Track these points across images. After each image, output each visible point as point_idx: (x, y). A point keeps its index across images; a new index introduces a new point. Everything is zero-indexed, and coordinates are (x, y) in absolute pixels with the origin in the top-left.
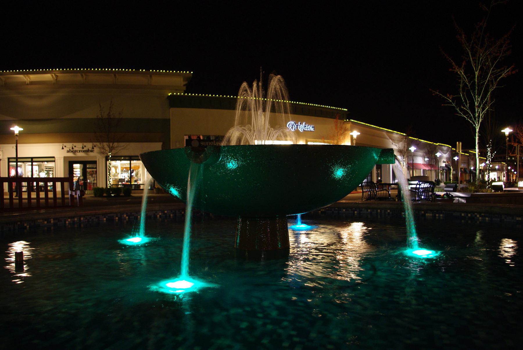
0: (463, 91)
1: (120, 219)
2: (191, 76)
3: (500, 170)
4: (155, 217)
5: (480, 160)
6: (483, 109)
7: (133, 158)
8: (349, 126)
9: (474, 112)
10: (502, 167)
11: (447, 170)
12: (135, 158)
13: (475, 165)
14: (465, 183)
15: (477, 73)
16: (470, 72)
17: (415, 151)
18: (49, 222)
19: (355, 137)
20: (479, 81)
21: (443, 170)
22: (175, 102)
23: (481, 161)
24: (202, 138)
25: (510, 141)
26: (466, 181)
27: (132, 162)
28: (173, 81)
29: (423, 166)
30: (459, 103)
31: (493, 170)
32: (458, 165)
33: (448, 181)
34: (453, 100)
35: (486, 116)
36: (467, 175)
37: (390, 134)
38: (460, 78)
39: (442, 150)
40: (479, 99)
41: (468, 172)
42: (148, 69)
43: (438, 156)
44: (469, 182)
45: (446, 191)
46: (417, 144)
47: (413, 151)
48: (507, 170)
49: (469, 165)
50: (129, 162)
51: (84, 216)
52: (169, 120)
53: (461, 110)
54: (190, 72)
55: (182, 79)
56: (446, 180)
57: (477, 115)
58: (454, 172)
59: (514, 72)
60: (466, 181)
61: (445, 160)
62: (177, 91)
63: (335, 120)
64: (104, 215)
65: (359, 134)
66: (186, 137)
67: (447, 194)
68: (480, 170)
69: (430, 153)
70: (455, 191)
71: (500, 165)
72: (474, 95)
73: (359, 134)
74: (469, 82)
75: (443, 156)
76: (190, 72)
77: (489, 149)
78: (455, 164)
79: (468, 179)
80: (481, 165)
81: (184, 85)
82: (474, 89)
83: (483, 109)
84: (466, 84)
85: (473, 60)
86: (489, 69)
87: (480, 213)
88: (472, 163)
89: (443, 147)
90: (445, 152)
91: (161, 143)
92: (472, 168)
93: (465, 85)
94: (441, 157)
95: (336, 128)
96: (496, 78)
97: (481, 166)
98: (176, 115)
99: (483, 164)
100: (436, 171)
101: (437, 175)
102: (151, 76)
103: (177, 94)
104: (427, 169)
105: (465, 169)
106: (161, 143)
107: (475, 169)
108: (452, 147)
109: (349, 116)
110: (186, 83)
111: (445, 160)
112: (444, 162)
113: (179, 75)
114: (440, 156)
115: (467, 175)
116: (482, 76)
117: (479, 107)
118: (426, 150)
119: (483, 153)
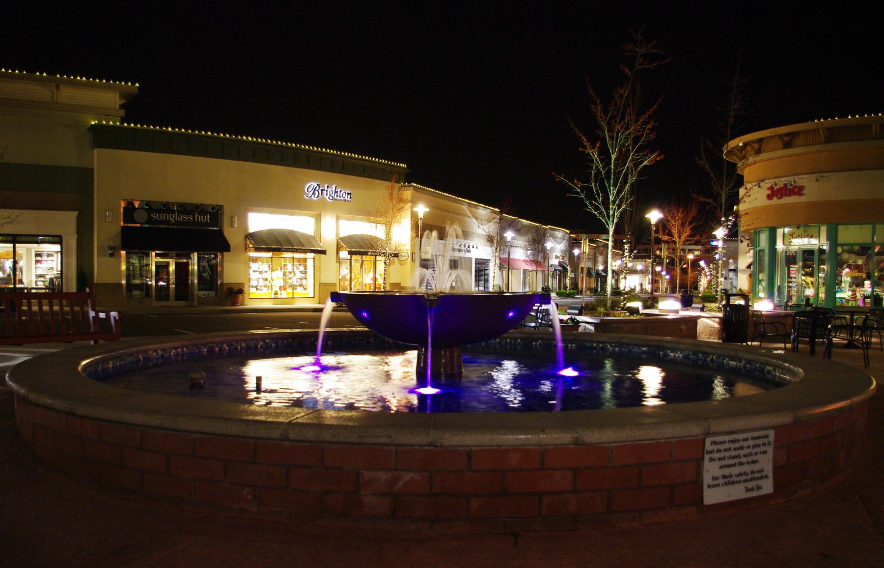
0: (595, 182)
1: (221, 350)
2: (136, 91)
3: (643, 272)
4: (256, 347)
5: (613, 253)
6: (619, 207)
7: (19, 239)
8: (408, 193)
9: (607, 209)
10: (646, 267)
11: (562, 271)
12: (24, 239)
13: (606, 263)
14: (588, 292)
15: (613, 157)
16: (606, 160)
17: (513, 238)
18: (157, 354)
19: (421, 215)
20: (616, 167)
21: (555, 270)
22: (103, 137)
23: (615, 255)
24: (137, 205)
25: (657, 232)
26: (590, 289)
27: (17, 245)
28: (101, 100)
29: (524, 264)
30: (591, 196)
31: (633, 271)
32: (578, 264)
33: (562, 291)
34: (582, 189)
35: (621, 218)
36: (593, 280)
37: (473, 209)
38: (592, 161)
39: (554, 237)
40: (615, 192)
41: (594, 274)
42: (51, 73)
43: (548, 248)
44: (594, 291)
45: (569, 314)
46: (519, 231)
47: (509, 239)
48: (654, 273)
49: (595, 262)
50: (10, 246)
51: (186, 347)
52: (91, 171)
53: (591, 204)
54: (133, 84)
55: (117, 96)
56: (559, 289)
57: (611, 213)
58: (573, 275)
59: (658, 159)
60: (590, 289)
61: (559, 254)
62: (107, 116)
63: (389, 184)
64: (205, 345)
65: (428, 210)
66: (123, 204)
67: (571, 319)
68: (613, 271)
69: (537, 243)
70: (580, 314)
71: (643, 263)
72: (609, 185)
73: (428, 210)
74: (604, 168)
75: (556, 245)
76: (133, 84)
77: (626, 246)
78: (574, 262)
79: (593, 286)
80: (614, 264)
81: (121, 107)
82: (609, 178)
83: (619, 207)
84: (599, 170)
85: (610, 137)
86: (628, 152)
87: (610, 343)
88: (600, 259)
89: (556, 233)
90: (560, 240)
91: (74, 215)
92: (601, 267)
93: (598, 172)
94: (552, 249)
95: (391, 199)
96: (636, 165)
97: (614, 264)
98: (102, 159)
99: (619, 262)
100: (543, 272)
101: (545, 279)
102: (58, 87)
103: (108, 122)
104: (530, 269)
105: (589, 270)
106: (77, 213)
107: (605, 270)
108: (571, 233)
109: (409, 178)
110: (123, 102)
111: (559, 254)
112: (557, 257)
113: (111, 88)
114: (552, 248)
115: (593, 280)
116: (622, 158)
117: (614, 202)
118: (530, 237)
119: (618, 245)
